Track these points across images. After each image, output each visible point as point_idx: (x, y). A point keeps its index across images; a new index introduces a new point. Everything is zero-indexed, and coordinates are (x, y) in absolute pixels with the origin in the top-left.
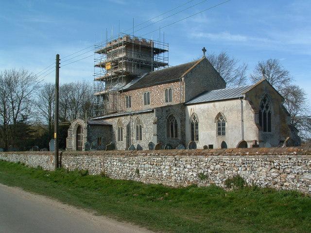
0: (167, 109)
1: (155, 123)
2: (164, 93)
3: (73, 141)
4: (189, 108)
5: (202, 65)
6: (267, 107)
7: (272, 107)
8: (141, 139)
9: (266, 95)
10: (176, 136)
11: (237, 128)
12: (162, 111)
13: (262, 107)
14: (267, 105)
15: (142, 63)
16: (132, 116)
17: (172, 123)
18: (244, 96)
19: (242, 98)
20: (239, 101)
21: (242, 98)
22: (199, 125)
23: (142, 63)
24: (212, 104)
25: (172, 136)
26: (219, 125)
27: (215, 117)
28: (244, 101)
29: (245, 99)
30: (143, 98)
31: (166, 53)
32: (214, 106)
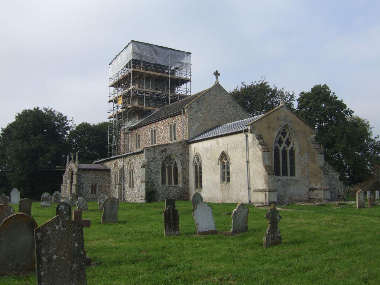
0: (162, 149)
1: (143, 167)
2: (169, 129)
3: (68, 189)
4: (193, 146)
5: (214, 92)
6: (288, 143)
7: (296, 143)
8: (133, 187)
9: (286, 126)
10: (176, 182)
11: (242, 172)
12: (155, 152)
13: (280, 142)
14: (288, 139)
15: (156, 95)
16: (125, 157)
17: (170, 167)
18: (249, 128)
19: (246, 131)
20: (243, 135)
21: (246, 131)
22: (203, 167)
23: (156, 95)
24: (214, 141)
25: (170, 183)
26: (223, 168)
27: (218, 157)
28: (250, 136)
29: (251, 132)
30: (150, 137)
31: (189, 83)
32: (218, 143)
